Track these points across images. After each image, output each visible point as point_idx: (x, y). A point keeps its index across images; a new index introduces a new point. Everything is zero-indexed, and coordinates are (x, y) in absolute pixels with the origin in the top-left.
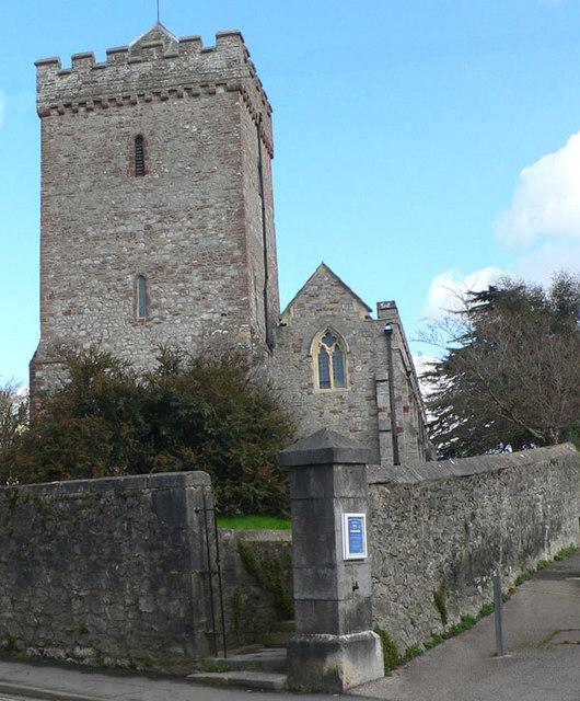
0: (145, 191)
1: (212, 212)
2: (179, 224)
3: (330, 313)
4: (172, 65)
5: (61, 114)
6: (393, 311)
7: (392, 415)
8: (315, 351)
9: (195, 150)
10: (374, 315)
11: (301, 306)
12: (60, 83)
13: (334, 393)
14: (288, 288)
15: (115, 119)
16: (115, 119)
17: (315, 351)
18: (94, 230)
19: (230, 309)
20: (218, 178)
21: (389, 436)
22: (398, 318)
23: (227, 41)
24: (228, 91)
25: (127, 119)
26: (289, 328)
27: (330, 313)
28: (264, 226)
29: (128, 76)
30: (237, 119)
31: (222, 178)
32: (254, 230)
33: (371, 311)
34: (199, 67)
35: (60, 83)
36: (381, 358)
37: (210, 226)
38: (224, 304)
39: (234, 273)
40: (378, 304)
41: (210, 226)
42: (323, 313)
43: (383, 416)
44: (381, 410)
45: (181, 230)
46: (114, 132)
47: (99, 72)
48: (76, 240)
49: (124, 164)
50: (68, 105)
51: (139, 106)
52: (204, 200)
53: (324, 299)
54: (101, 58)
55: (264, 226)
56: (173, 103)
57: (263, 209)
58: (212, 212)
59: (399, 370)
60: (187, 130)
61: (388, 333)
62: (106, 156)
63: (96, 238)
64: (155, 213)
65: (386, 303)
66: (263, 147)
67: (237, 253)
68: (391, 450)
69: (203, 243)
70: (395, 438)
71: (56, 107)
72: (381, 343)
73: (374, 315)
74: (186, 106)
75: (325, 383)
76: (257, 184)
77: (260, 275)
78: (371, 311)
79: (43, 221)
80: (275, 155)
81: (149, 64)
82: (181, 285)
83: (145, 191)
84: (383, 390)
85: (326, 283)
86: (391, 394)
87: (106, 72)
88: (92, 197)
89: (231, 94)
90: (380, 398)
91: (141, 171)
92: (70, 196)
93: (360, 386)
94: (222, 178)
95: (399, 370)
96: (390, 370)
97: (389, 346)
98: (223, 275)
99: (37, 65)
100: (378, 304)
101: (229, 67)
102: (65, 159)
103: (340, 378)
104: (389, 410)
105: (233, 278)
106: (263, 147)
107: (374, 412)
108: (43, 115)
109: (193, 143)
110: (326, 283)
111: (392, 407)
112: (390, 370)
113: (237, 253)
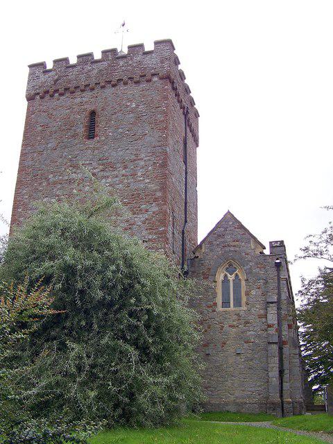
0: (94, 149)
1: (142, 163)
2: (116, 172)
3: (232, 249)
4: (121, 63)
5: (42, 98)
6: (282, 249)
7: (279, 331)
8: (220, 277)
9: (133, 120)
10: (267, 252)
11: (210, 243)
12: (43, 78)
13: (233, 311)
14: (203, 229)
15: (78, 100)
16: (78, 100)
17: (220, 277)
18: (54, 177)
19: (150, 237)
20: (148, 139)
21: (275, 347)
22: (285, 254)
23: (161, 46)
24: (161, 79)
25: (87, 101)
26: (201, 260)
27: (232, 249)
28: (186, 185)
29: (90, 71)
30: (166, 98)
31: (152, 138)
32: (176, 180)
33: (265, 248)
34: (140, 63)
35: (43, 78)
36: (273, 284)
37: (139, 174)
38: (144, 233)
39: (156, 209)
40: (271, 243)
41: (139, 174)
42: (227, 249)
43: (272, 331)
44: (269, 326)
45: (117, 177)
46: (76, 109)
47: (71, 70)
48: (40, 184)
49: (81, 130)
50: (47, 92)
51: (96, 91)
52: (136, 155)
53: (228, 238)
54: (73, 61)
55: (186, 185)
56: (121, 87)
57: (186, 173)
58: (142, 163)
59: (284, 296)
60: (127, 106)
61: (278, 265)
62: (69, 125)
63: (55, 183)
64: (99, 164)
65: (277, 242)
66: (188, 129)
67: (159, 194)
68: (277, 359)
69: (132, 187)
70: (281, 349)
71: (38, 94)
72: (272, 272)
73: (267, 252)
74: (132, 90)
75: (226, 303)
76: (182, 152)
77: (180, 215)
78: (265, 248)
79: (20, 171)
80: (200, 144)
81: (105, 63)
82: (113, 218)
83: (94, 149)
84: (272, 311)
85: (229, 226)
86: (279, 314)
87: (75, 69)
88: (57, 152)
89: (161, 82)
90: (270, 316)
91: (91, 133)
92: (41, 153)
93: (254, 306)
94: (152, 138)
95: (284, 296)
96: (279, 295)
97: (278, 276)
98: (147, 211)
99: (93, 113)
100: (271, 243)
101: (162, 62)
102: (40, 128)
103: (238, 303)
104: (276, 326)
105: (154, 213)
106: (188, 129)
107: (264, 327)
108: (30, 98)
109: (131, 115)
110: (229, 226)
111: (279, 324)
112: (279, 295)
113: (159, 194)
